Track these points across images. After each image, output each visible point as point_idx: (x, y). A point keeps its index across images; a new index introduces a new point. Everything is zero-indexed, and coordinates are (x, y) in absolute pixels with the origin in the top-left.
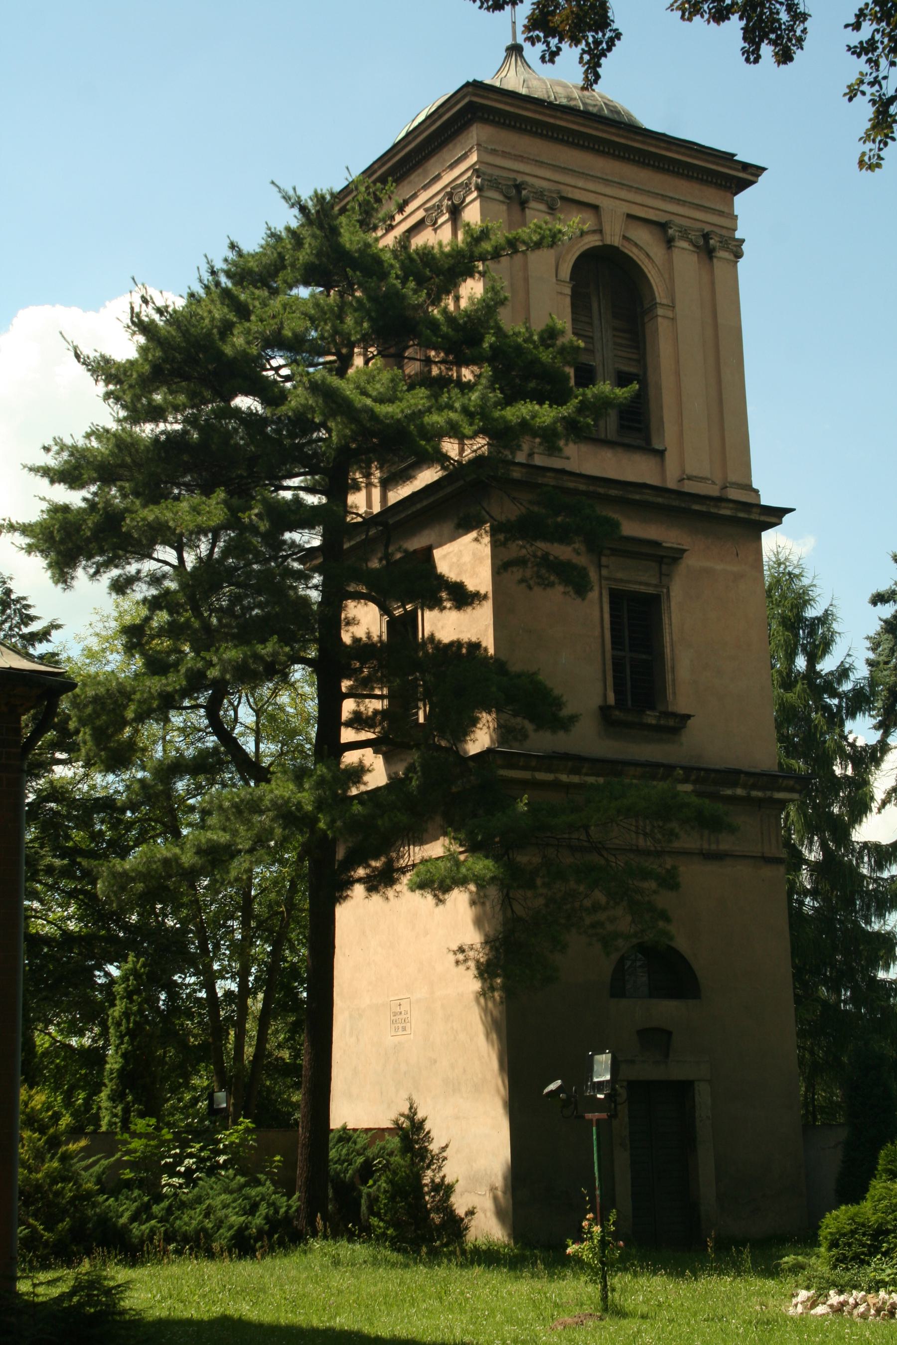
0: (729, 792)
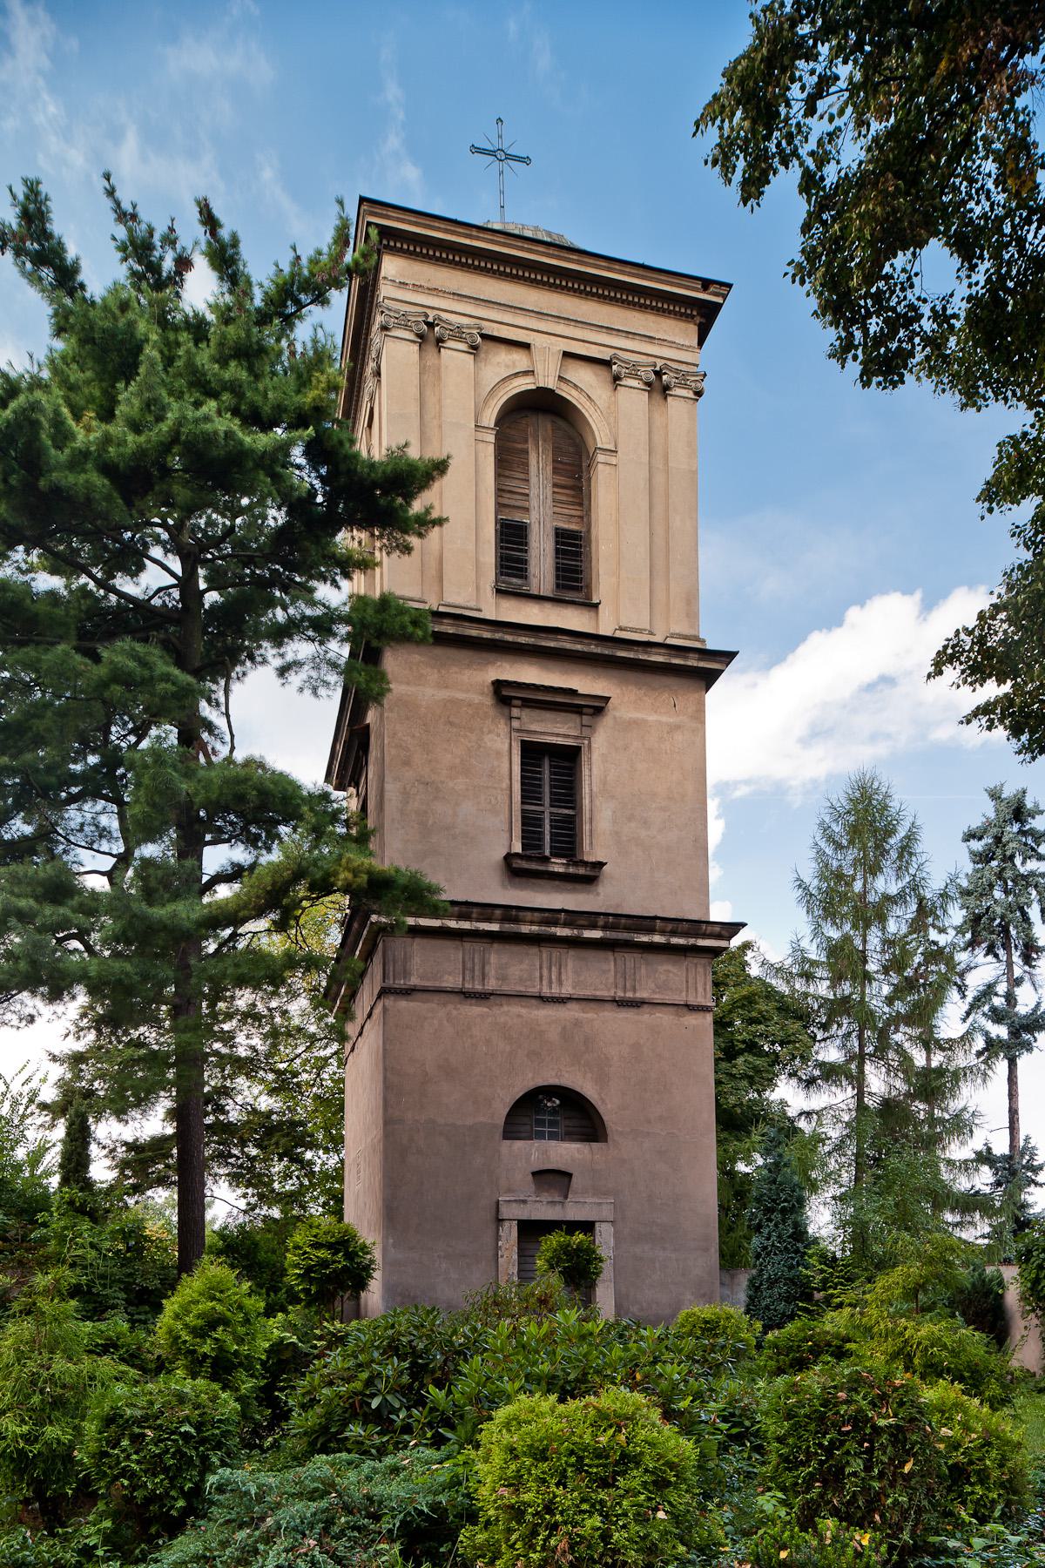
0: (645, 939)
